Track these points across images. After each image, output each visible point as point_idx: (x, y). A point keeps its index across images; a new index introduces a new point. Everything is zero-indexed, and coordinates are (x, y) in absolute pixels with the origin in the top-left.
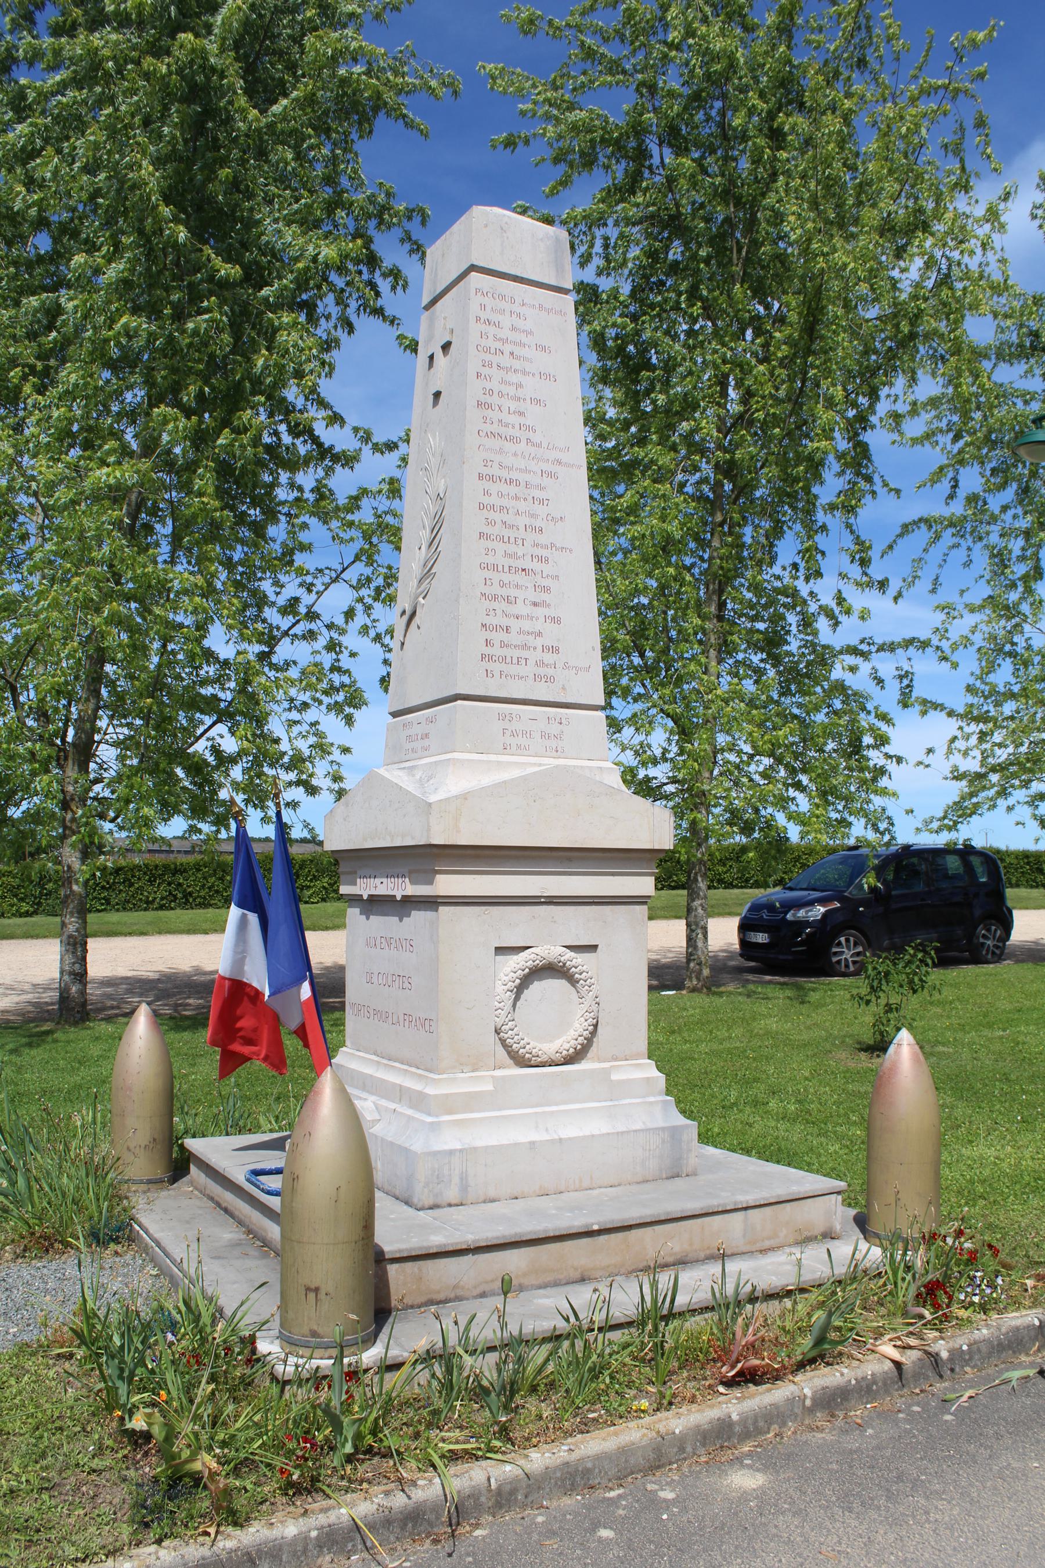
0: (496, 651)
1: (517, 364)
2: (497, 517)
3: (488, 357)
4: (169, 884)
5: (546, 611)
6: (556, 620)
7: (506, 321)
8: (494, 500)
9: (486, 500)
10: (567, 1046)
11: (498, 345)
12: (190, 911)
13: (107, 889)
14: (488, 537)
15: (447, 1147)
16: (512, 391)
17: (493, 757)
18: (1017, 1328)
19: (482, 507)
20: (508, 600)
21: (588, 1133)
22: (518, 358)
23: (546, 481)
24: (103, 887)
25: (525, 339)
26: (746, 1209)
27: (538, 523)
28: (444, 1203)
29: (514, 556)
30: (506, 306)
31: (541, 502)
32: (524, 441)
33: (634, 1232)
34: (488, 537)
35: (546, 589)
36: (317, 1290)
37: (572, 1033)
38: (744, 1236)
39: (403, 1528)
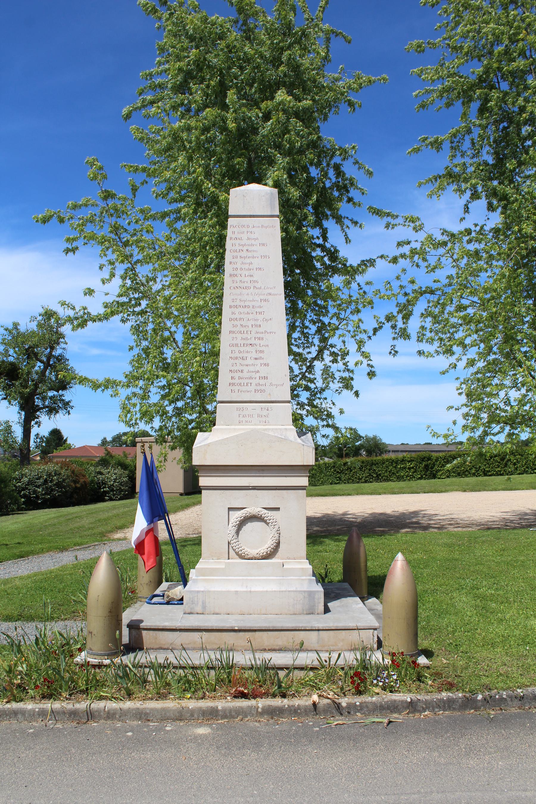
0: (236, 381)
1: (250, 254)
2: (238, 323)
3: (235, 254)
4: (370, 470)
5: (262, 361)
6: (267, 365)
7: (245, 236)
8: (237, 316)
9: (233, 317)
10: (262, 551)
11: (241, 248)
12: (381, 483)
13: (340, 473)
14: (233, 332)
15: (197, 589)
16: (247, 266)
17: (233, 427)
18: (395, 701)
19: (231, 320)
20: (243, 358)
21: (265, 590)
22: (251, 251)
23: (263, 303)
24: (338, 472)
25: (253, 242)
26: (318, 630)
27: (258, 323)
28: (195, 612)
29: (247, 339)
30: (245, 230)
31: (260, 313)
32: (252, 288)
33: (257, 633)
34: (233, 332)
35: (261, 352)
36: (91, 633)
37: (267, 546)
38: (318, 643)
39: (70, 716)
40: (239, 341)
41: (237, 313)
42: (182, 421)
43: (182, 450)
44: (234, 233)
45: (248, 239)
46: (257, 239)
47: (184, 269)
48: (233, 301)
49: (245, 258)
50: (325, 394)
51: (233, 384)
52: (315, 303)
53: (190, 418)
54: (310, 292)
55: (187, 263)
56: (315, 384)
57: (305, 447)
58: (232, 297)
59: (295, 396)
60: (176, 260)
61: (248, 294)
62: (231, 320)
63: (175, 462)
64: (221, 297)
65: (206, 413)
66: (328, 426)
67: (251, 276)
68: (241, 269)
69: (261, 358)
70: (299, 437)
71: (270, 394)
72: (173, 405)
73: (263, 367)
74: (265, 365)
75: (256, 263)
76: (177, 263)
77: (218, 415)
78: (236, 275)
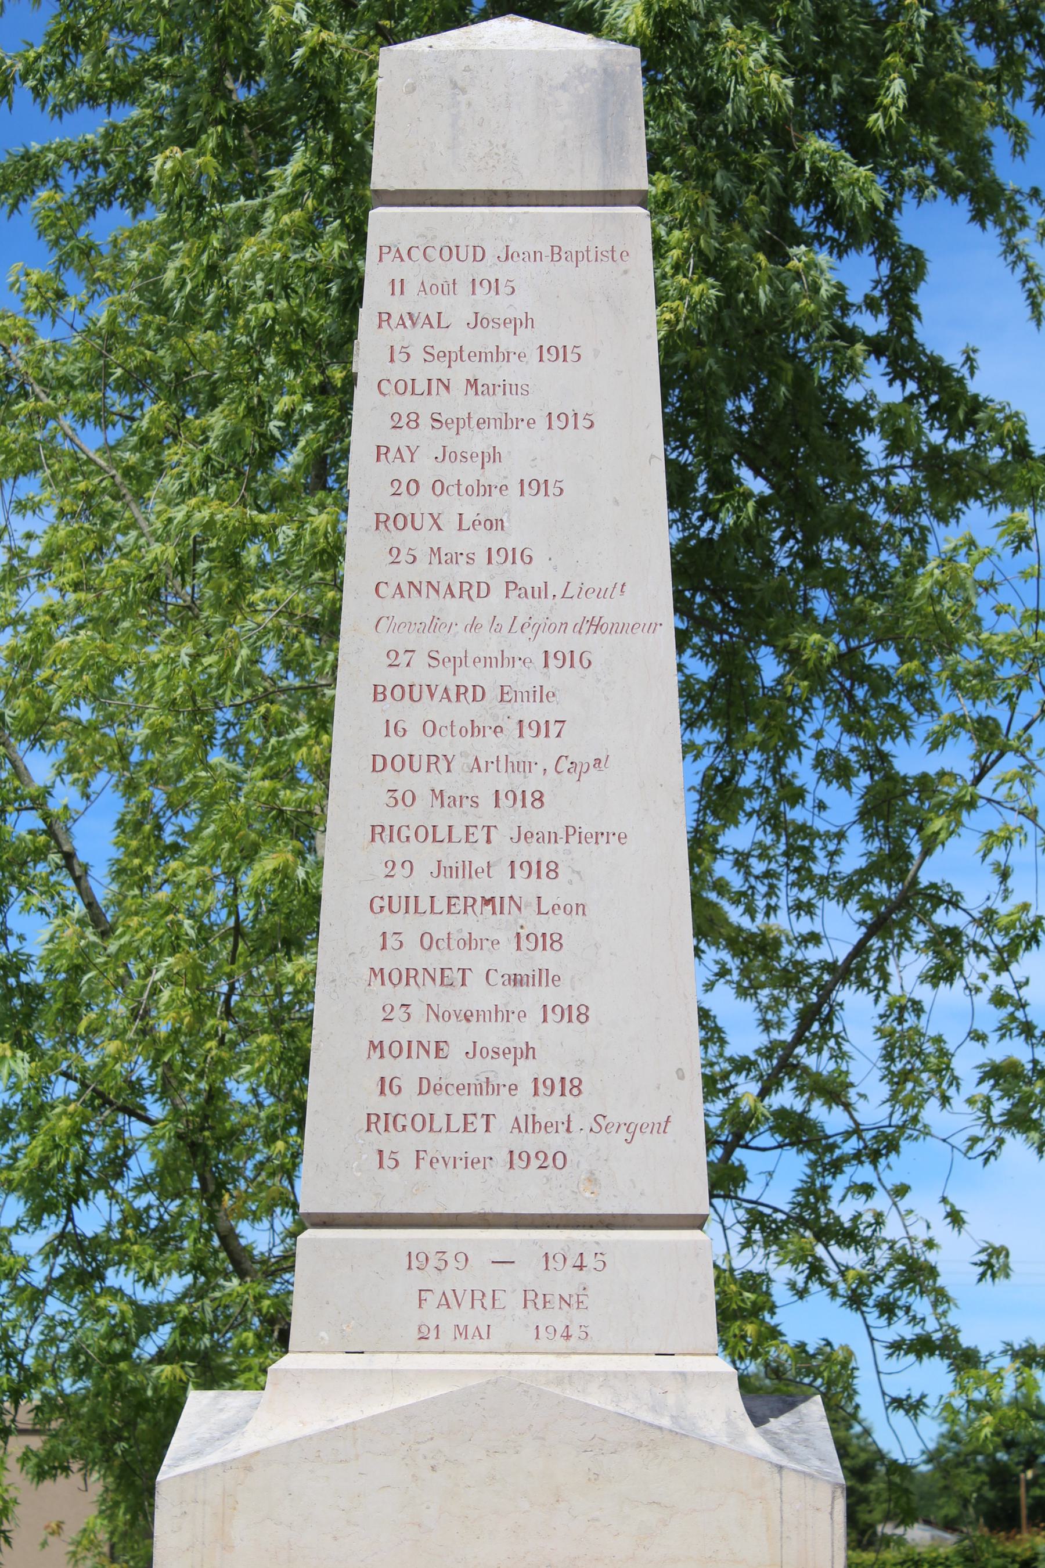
0: (409, 1103)
1: (486, 406)
2: (421, 782)
3: (406, 404)
5: (549, 995)
6: (576, 1014)
7: (458, 308)
8: (415, 744)
9: (391, 747)
11: (438, 370)
14: (394, 833)
16: (469, 473)
20: (443, 977)
22: (490, 390)
23: (558, 677)
25: (505, 338)
27: (532, 783)
29: (467, 871)
30: (461, 271)
31: (542, 729)
34: (394, 833)
35: (550, 941)
40: (423, 884)
41: (414, 728)
42: (101, 1314)
43: (97, 1482)
44: (398, 287)
45: (479, 321)
46: (528, 322)
47: (127, 472)
48: (398, 488)
49: (459, 425)
50: (896, 1168)
51: (391, 1122)
52: (851, 664)
53: (146, 1296)
54: (822, 604)
55: (145, 441)
56: (847, 1106)
57: (791, 1482)
58: (391, 640)
59: (725, 1180)
60: (83, 417)
61: (474, 626)
62: (379, 764)
63: (60, 1547)
64: (327, 626)
65: (242, 1273)
66: (922, 1347)
67: (495, 524)
68: (439, 487)
69: (544, 977)
70: (758, 1420)
71: (592, 1179)
72: (53, 1225)
73: (557, 1030)
74: (567, 1013)
75: (524, 452)
76: (91, 440)
77: (304, 1285)
78: (409, 521)
